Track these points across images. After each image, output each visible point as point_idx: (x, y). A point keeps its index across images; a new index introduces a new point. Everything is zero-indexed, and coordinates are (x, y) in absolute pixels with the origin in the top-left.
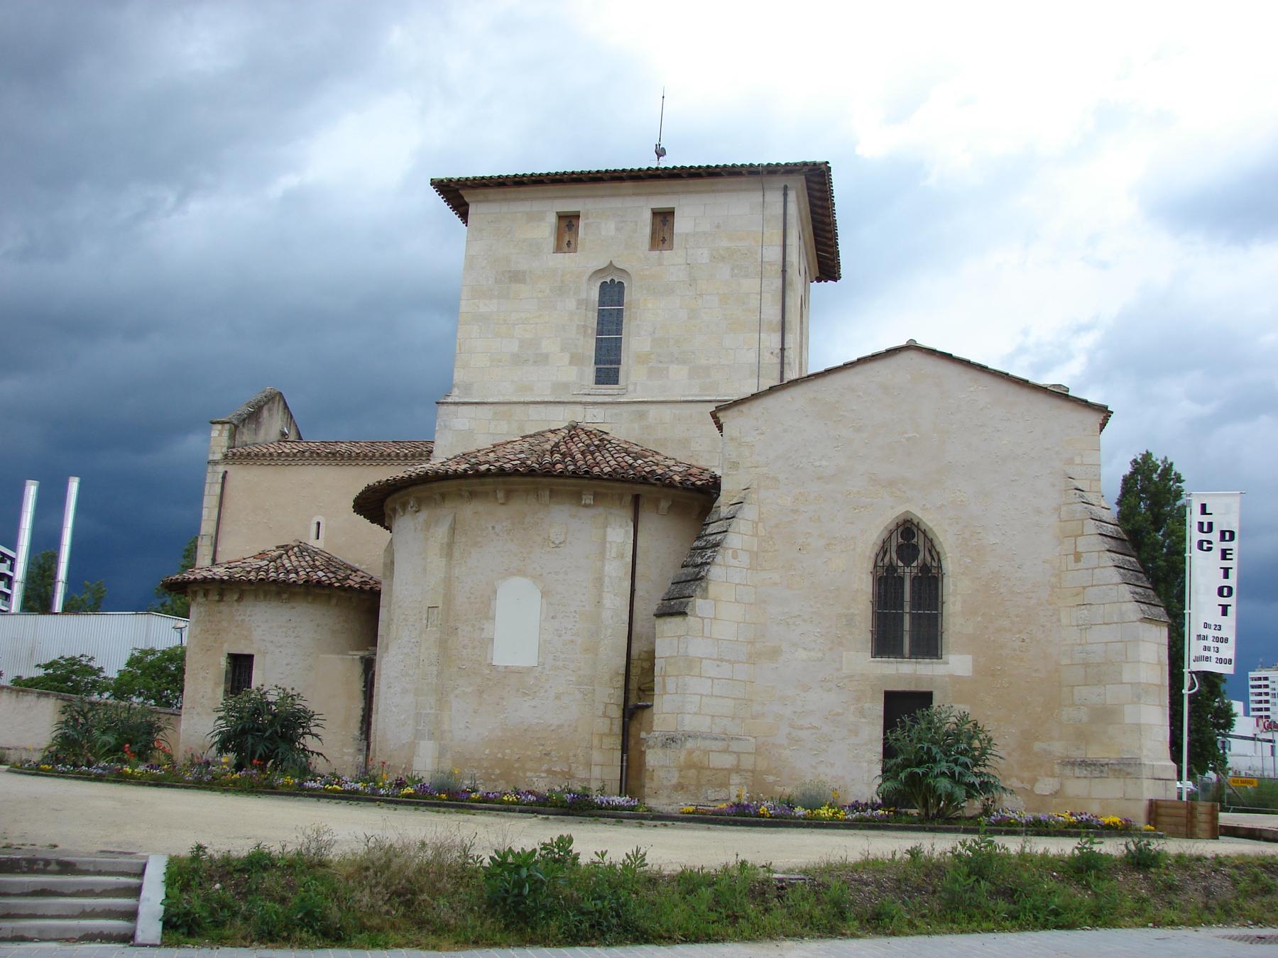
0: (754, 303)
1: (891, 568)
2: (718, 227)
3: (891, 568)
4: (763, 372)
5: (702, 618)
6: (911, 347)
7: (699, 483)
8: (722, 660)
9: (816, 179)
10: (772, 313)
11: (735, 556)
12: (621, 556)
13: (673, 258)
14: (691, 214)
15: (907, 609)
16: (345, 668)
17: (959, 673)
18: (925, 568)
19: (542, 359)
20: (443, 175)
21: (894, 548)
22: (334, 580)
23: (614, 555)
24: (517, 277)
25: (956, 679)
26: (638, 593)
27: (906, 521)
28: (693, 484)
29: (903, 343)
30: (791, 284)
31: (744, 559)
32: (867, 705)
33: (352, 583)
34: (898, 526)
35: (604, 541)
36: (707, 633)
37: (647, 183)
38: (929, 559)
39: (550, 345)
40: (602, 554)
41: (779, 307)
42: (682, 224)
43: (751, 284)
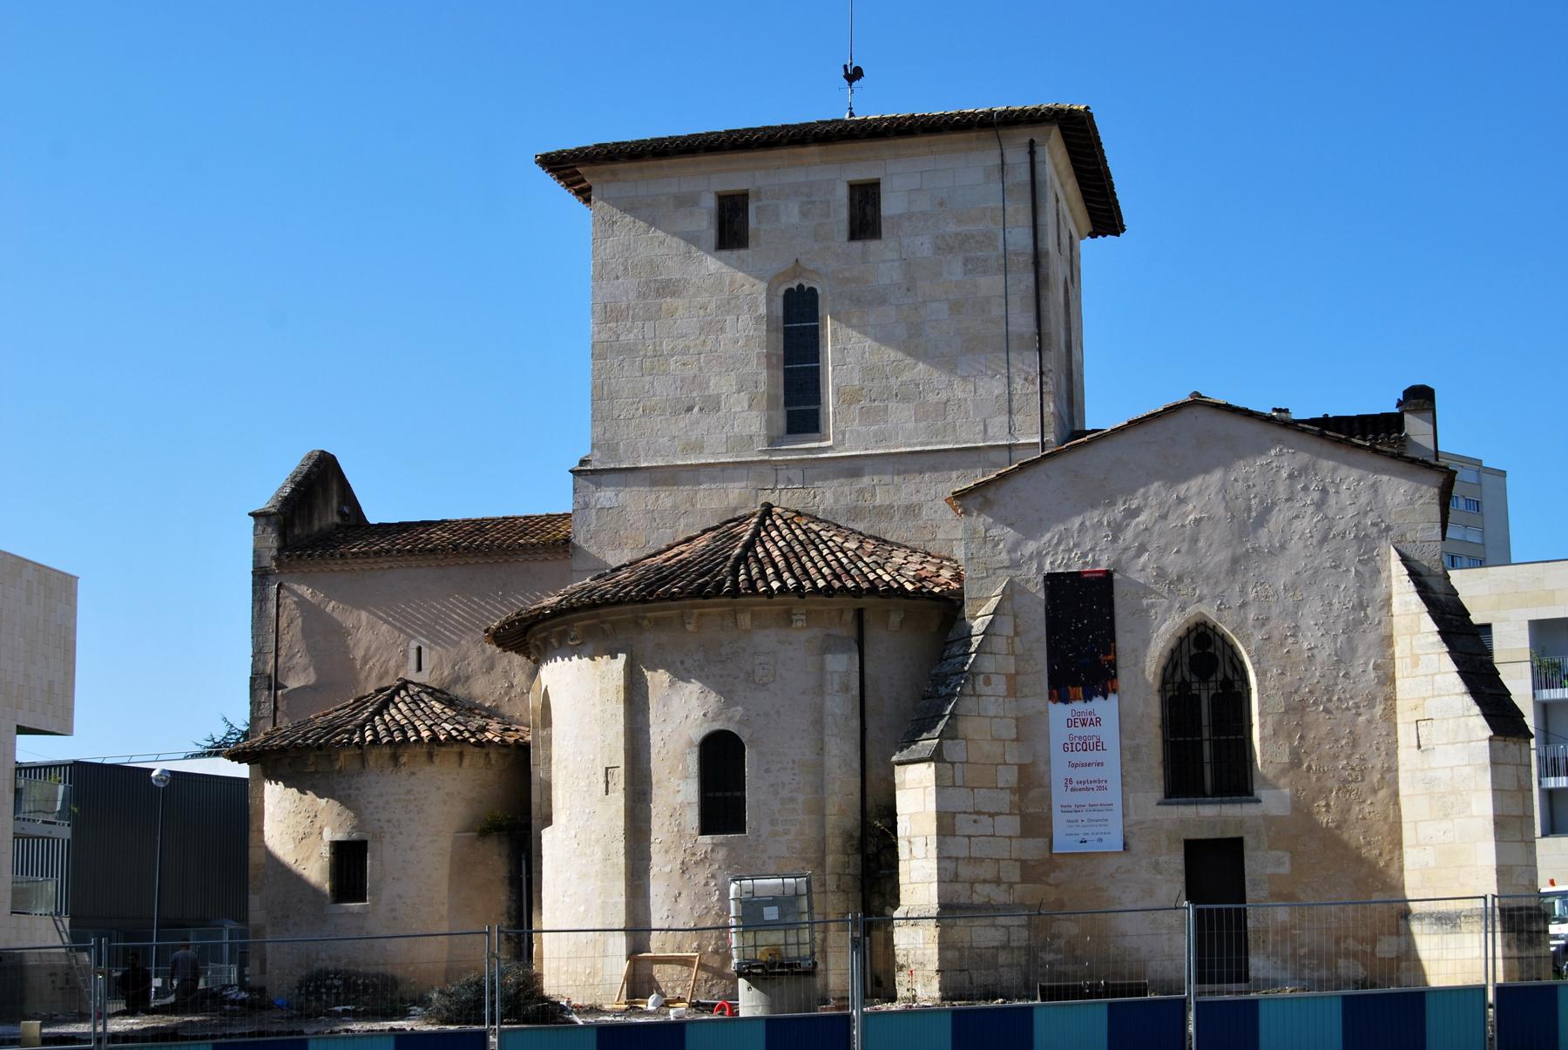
0: (997, 311)
1: (1185, 685)
2: (941, 204)
3: (1185, 685)
4: (1015, 405)
5: (953, 763)
6: (1197, 402)
7: (937, 590)
8: (979, 813)
9: (1078, 132)
10: (1023, 322)
11: (987, 682)
12: (846, 688)
13: (881, 260)
14: (903, 181)
15: (1206, 734)
16: (926, 754)
17: (1274, 812)
18: (1227, 684)
19: (712, 404)
20: (552, 147)
21: (1186, 660)
22: (467, 734)
23: (836, 687)
24: (668, 288)
25: (1270, 820)
26: (870, 735)
27: (1197, 625)
28: (930, 592)
29: (1183, 396)
30: (1047, 281)
31: (999, 685)
32: (1162, 859)
33: (490, 736)
34: (1189, 631)
35: (822, 668)
36: (959, 782)
37: (838, 147)
38: (1229, 673)
39: (722, 384)
40: (820, 689)
41: (1032, 314)
42: (890, 205)
43: (991, 284)
